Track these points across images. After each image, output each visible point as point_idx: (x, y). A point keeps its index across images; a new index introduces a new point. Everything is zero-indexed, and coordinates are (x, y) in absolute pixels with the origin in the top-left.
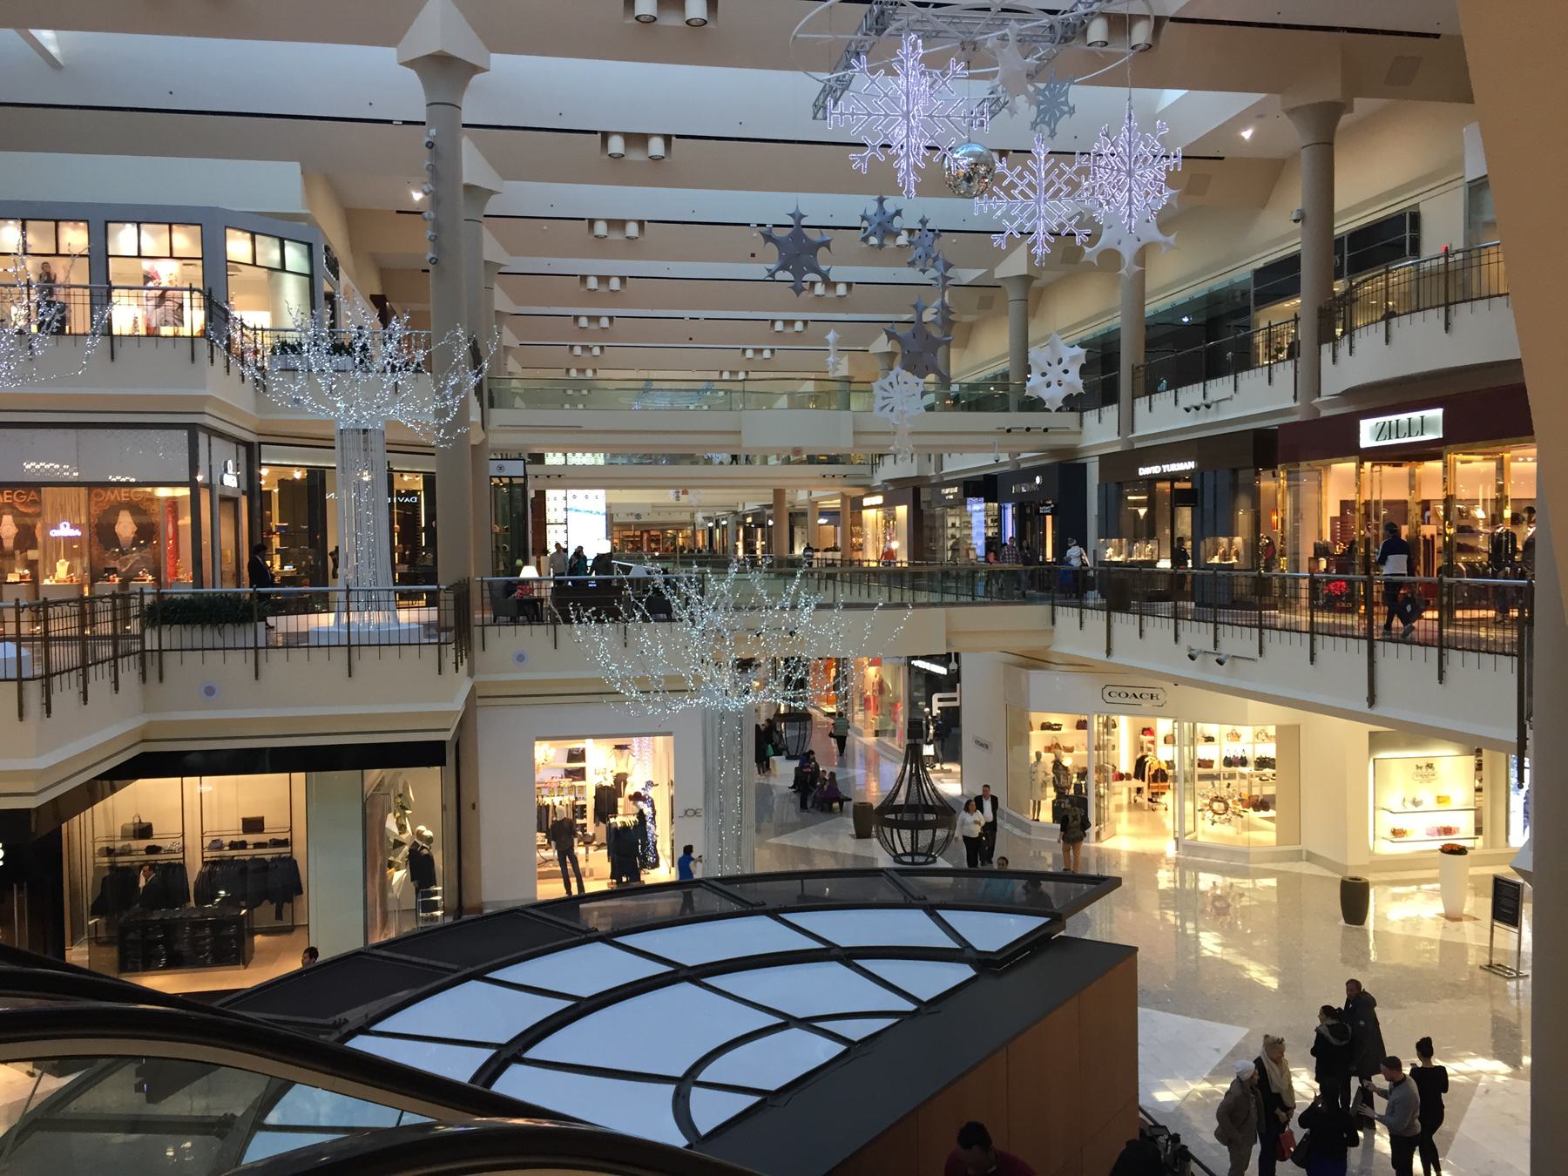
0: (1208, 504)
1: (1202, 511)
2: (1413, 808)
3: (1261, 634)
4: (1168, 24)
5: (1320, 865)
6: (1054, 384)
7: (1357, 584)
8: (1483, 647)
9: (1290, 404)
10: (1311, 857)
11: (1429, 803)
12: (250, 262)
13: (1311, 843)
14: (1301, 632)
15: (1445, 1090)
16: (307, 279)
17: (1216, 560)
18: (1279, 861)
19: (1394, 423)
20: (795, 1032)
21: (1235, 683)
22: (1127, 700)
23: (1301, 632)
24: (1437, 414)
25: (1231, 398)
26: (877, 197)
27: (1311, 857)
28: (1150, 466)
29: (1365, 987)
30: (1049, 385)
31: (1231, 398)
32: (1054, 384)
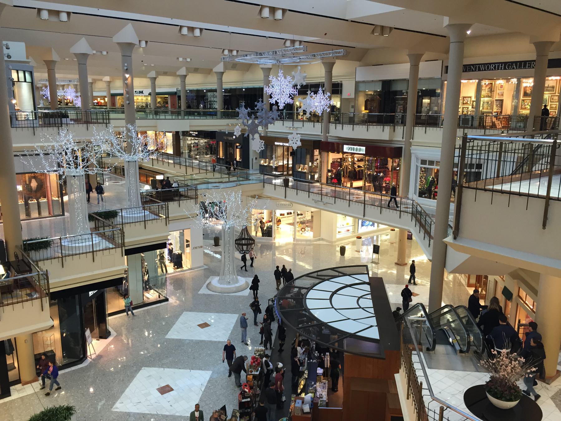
0: (299, 156)
1: (297, 157)
2: (343, 227)
3: (335, 199)
4: (303, 42)
5: (325, 241)
6: (297, 142)
7: (216, 117)
8: (394, 209)
9: (320, 134)
10: (322, 239)
11: (345, 225)
12: (17, 81)
13: (323, 236)
14: (346, 200)
15: (259, 282)
16: (30, 83)
17: (300, 170)
18: (316, 241)
19: (353, 148)
20: (361, 309)
21: (327, 209)
22: (283, 206)
23: (346, 200)
24: (364, 148)
25: (301, 128)
26: (274, 103)
27: (322, 239)
28: (279, 142)
29: (535, 296)
30: (296, 143)
31: (301, 128)
32: (297, 142)
